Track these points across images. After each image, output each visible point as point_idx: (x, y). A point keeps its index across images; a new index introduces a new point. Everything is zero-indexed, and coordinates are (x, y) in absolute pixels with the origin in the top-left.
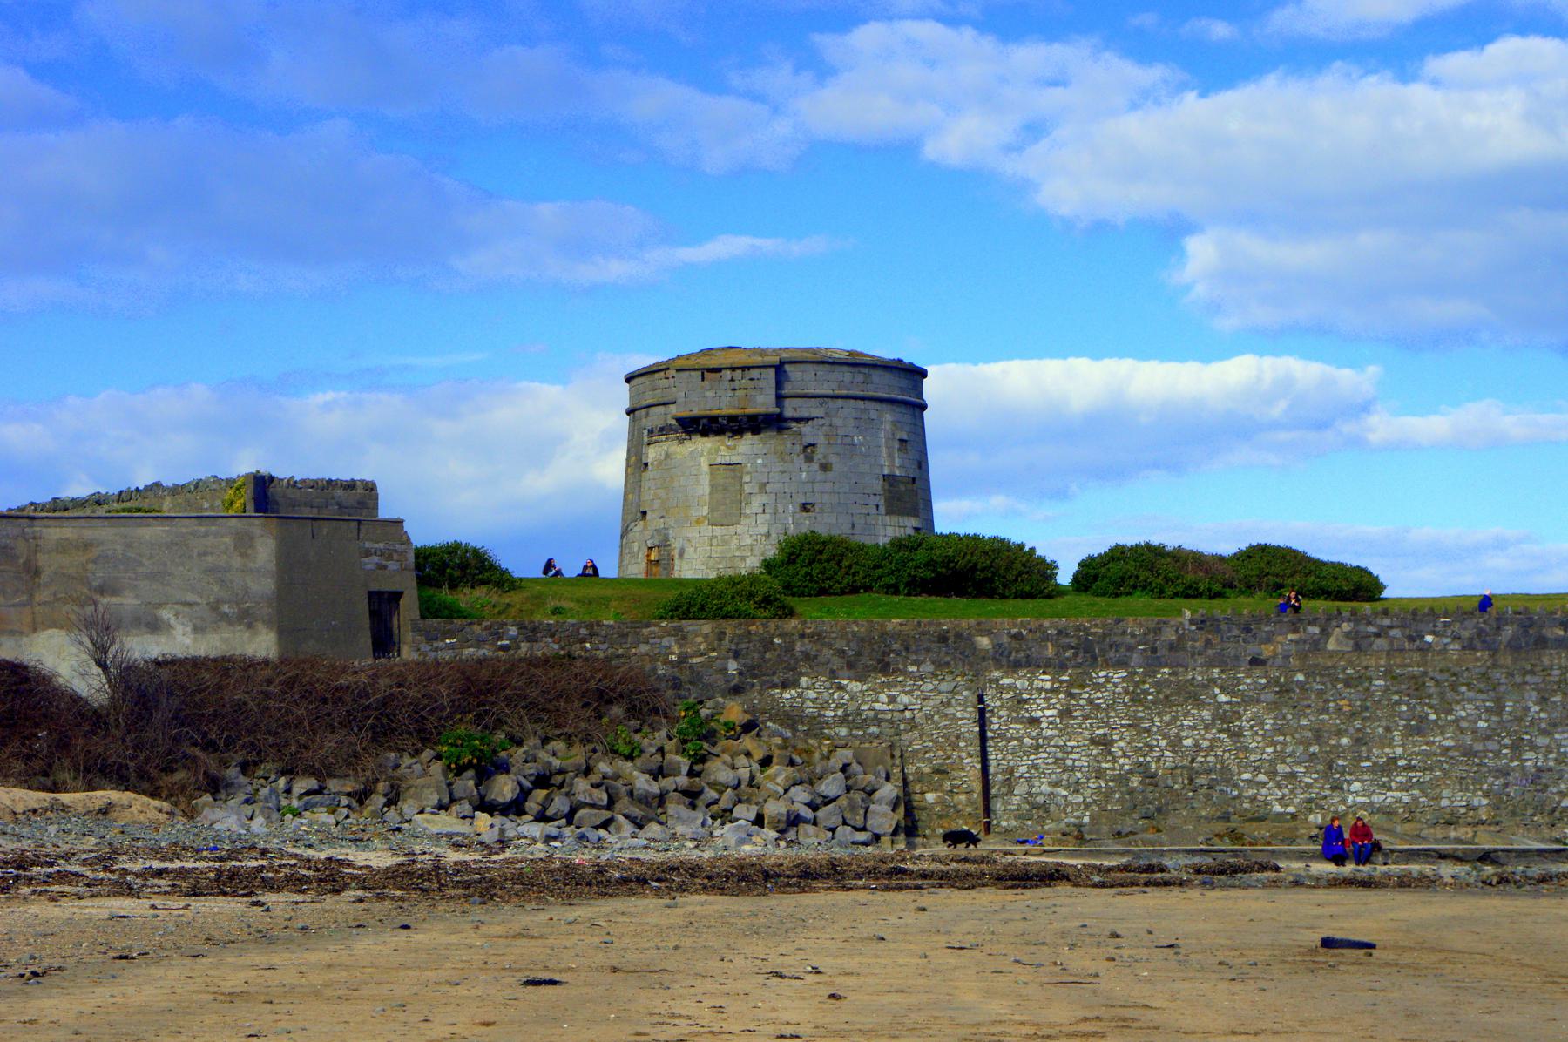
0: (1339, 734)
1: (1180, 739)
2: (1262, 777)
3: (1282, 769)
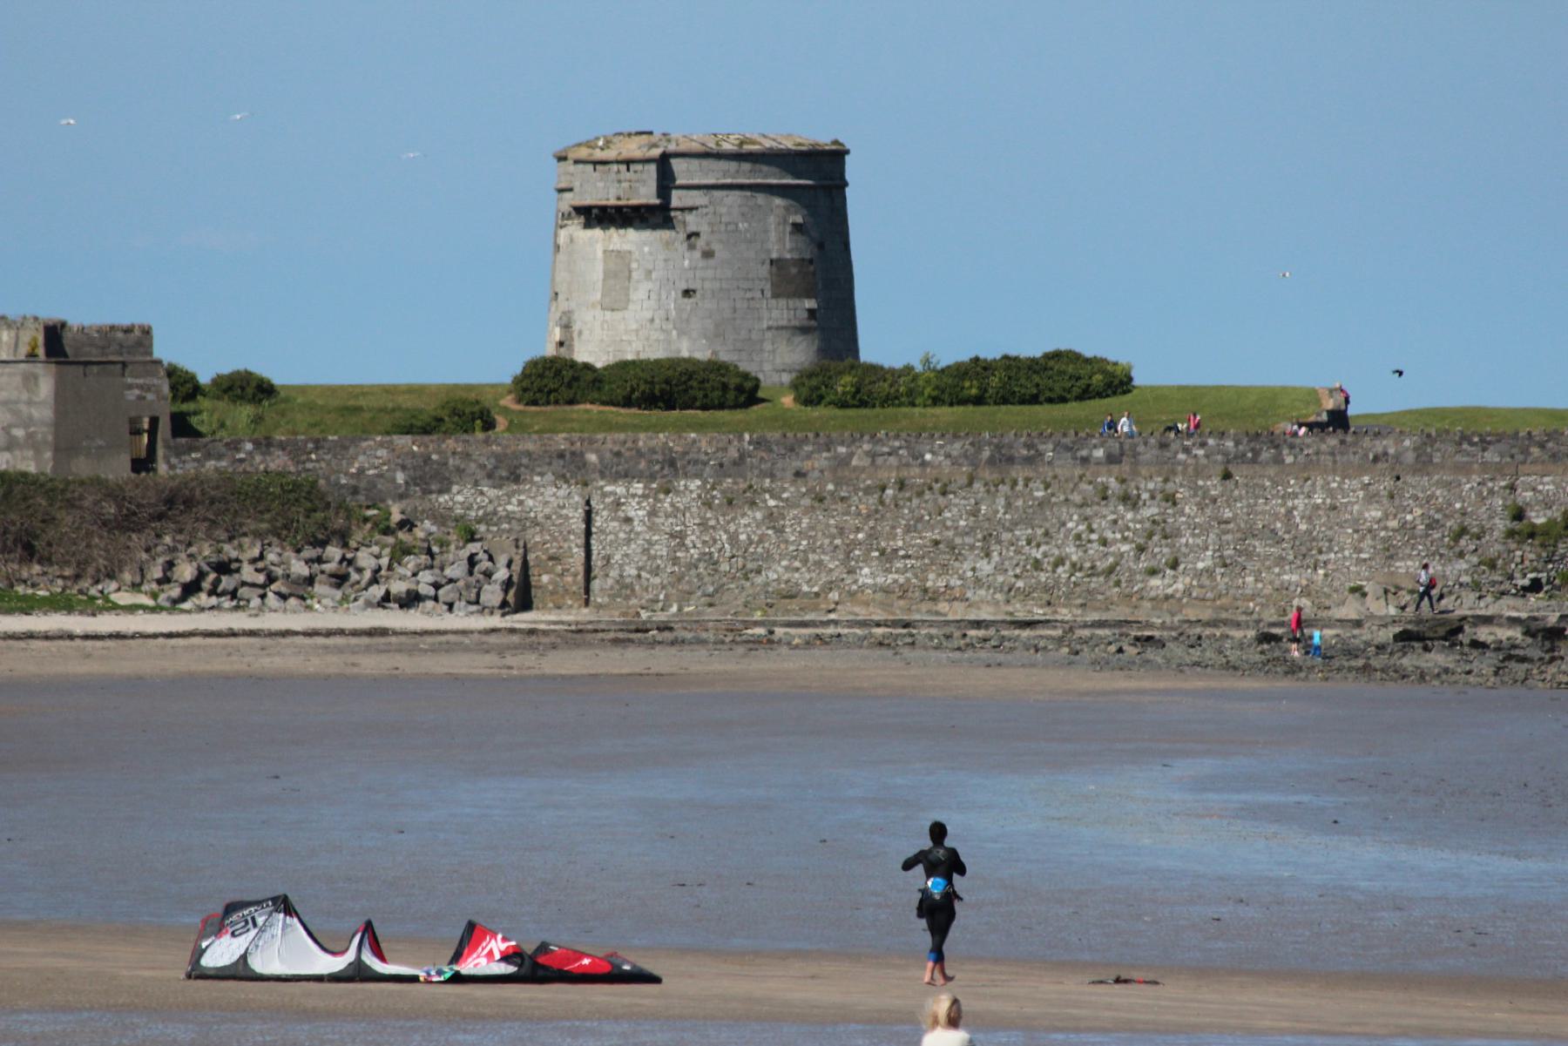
0: (858, 530)
1: (736, 533)
2: (797, 564)
3: (812, 557)
